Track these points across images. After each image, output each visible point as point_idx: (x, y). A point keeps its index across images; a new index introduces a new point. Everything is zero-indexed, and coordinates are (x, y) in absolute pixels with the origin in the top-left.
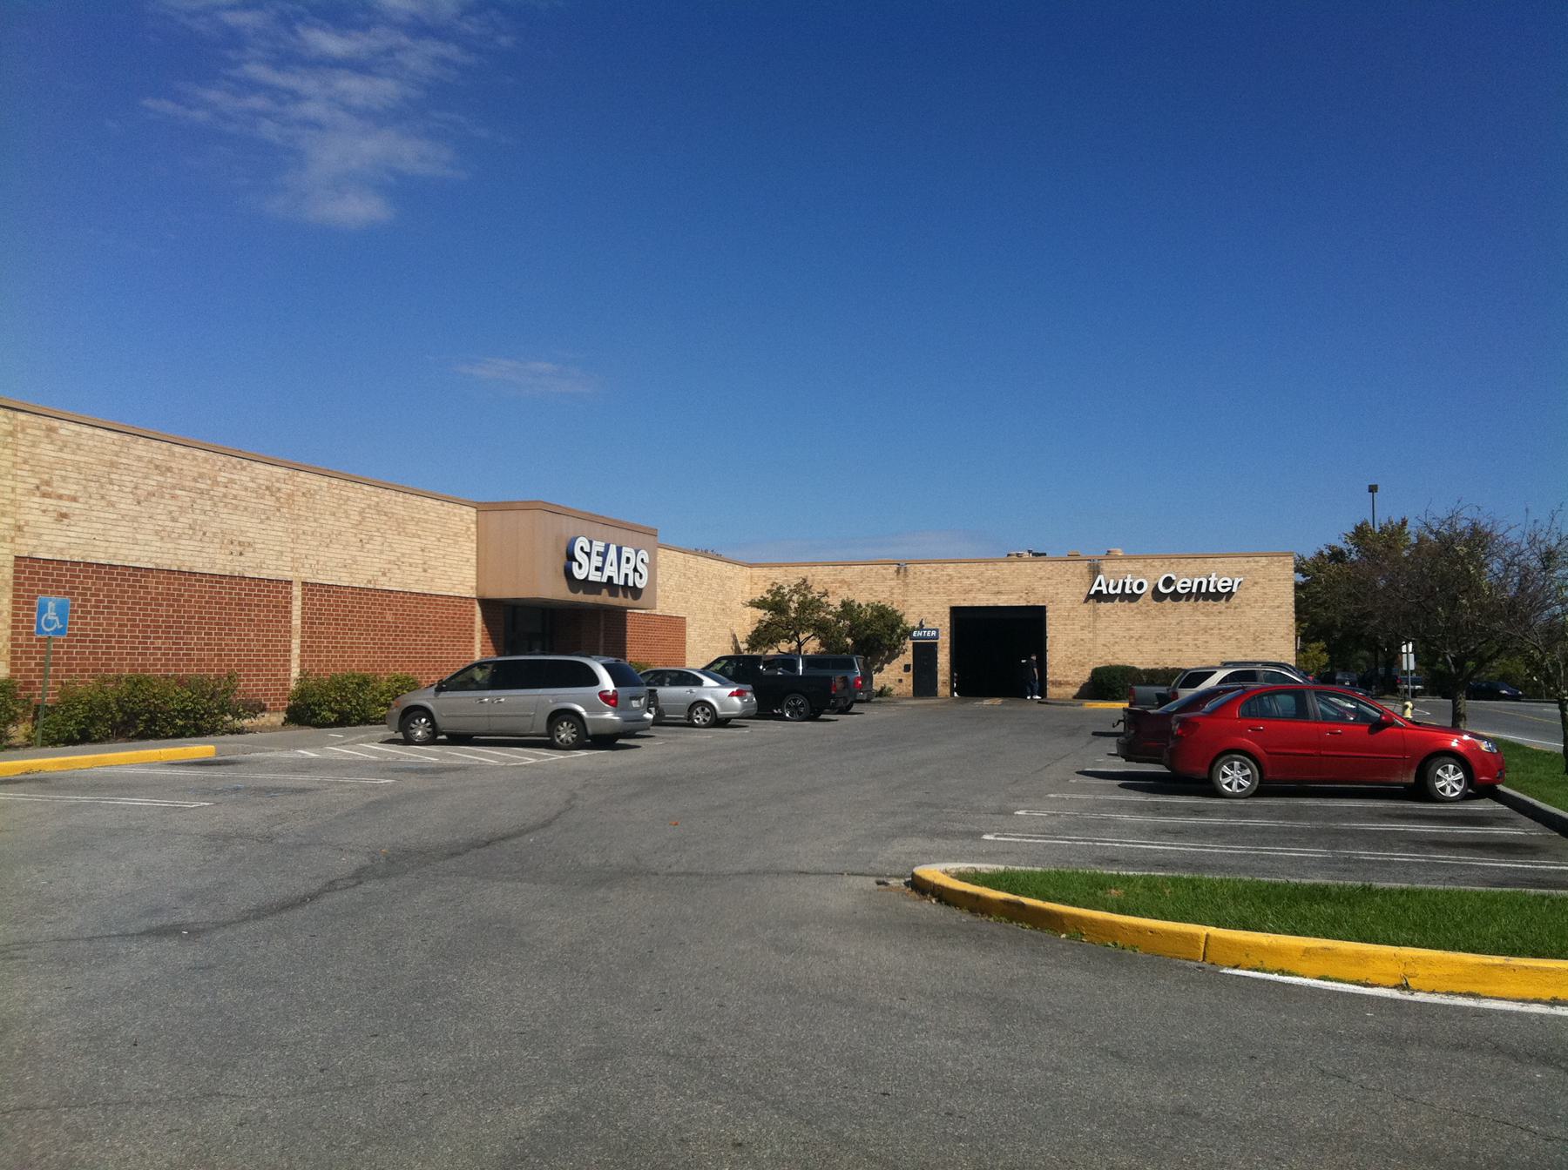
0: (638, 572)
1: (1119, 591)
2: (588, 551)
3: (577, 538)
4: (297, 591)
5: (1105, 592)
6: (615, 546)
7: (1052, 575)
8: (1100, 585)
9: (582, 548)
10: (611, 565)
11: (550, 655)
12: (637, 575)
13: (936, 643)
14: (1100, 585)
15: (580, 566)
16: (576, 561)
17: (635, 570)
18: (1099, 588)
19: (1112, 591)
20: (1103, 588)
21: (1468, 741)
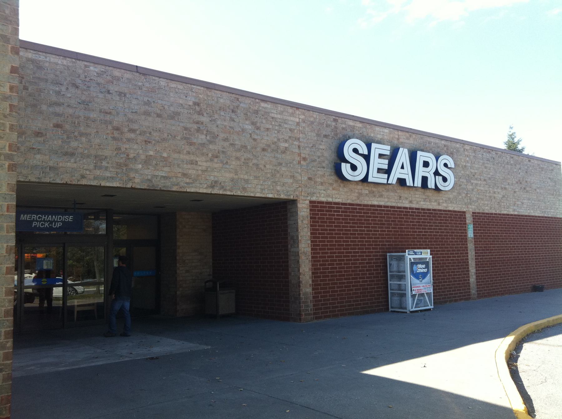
0: (439, 175)
1: (59, 223)
2: (366, 153)
3: (349, 138)
4: (23, 217)
5: (51, 220)
6: (406, 151)
7: (313, 194)
8: (50, 218)
9: (355, 151)
10: (402, 167)
11: (408, 272)
12: (439, 179)
13: (475, 215)
14: (50, 218)
15: (354, 168)
16: (347, 162)
17: (437, 173)
18: (50, 219)
19: (58, 220)
20: (51, 219)
21: (47, 301)
